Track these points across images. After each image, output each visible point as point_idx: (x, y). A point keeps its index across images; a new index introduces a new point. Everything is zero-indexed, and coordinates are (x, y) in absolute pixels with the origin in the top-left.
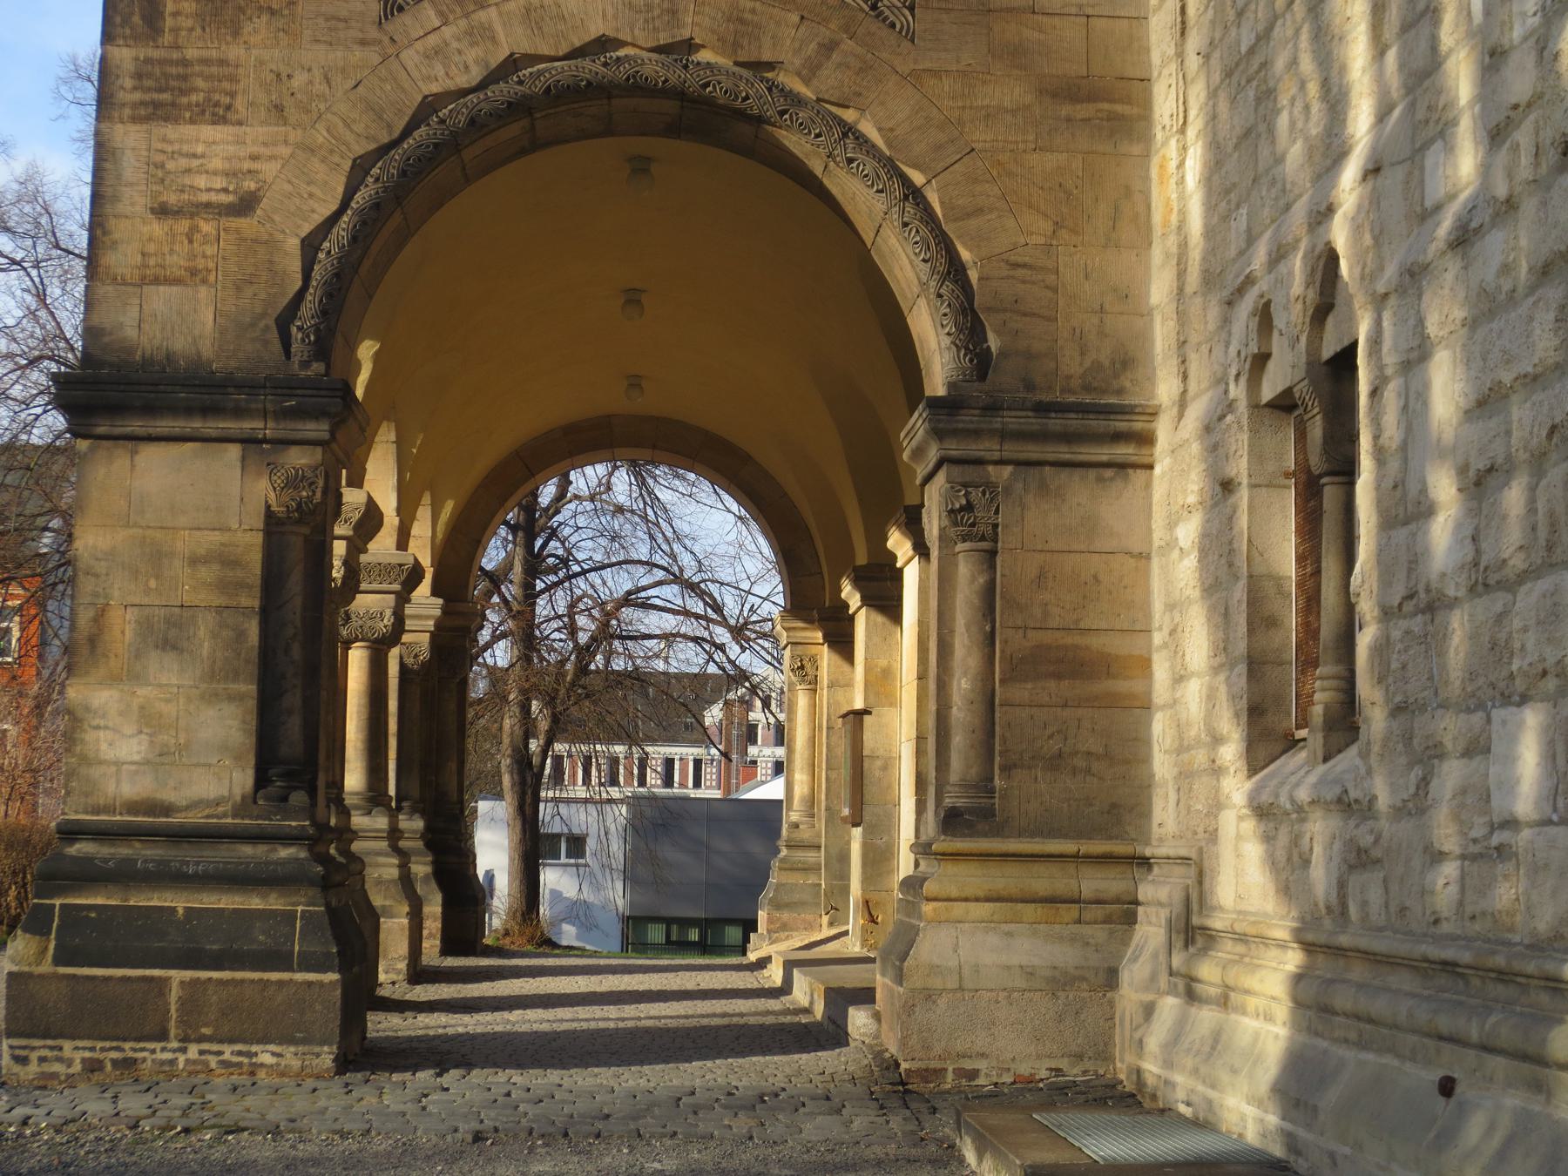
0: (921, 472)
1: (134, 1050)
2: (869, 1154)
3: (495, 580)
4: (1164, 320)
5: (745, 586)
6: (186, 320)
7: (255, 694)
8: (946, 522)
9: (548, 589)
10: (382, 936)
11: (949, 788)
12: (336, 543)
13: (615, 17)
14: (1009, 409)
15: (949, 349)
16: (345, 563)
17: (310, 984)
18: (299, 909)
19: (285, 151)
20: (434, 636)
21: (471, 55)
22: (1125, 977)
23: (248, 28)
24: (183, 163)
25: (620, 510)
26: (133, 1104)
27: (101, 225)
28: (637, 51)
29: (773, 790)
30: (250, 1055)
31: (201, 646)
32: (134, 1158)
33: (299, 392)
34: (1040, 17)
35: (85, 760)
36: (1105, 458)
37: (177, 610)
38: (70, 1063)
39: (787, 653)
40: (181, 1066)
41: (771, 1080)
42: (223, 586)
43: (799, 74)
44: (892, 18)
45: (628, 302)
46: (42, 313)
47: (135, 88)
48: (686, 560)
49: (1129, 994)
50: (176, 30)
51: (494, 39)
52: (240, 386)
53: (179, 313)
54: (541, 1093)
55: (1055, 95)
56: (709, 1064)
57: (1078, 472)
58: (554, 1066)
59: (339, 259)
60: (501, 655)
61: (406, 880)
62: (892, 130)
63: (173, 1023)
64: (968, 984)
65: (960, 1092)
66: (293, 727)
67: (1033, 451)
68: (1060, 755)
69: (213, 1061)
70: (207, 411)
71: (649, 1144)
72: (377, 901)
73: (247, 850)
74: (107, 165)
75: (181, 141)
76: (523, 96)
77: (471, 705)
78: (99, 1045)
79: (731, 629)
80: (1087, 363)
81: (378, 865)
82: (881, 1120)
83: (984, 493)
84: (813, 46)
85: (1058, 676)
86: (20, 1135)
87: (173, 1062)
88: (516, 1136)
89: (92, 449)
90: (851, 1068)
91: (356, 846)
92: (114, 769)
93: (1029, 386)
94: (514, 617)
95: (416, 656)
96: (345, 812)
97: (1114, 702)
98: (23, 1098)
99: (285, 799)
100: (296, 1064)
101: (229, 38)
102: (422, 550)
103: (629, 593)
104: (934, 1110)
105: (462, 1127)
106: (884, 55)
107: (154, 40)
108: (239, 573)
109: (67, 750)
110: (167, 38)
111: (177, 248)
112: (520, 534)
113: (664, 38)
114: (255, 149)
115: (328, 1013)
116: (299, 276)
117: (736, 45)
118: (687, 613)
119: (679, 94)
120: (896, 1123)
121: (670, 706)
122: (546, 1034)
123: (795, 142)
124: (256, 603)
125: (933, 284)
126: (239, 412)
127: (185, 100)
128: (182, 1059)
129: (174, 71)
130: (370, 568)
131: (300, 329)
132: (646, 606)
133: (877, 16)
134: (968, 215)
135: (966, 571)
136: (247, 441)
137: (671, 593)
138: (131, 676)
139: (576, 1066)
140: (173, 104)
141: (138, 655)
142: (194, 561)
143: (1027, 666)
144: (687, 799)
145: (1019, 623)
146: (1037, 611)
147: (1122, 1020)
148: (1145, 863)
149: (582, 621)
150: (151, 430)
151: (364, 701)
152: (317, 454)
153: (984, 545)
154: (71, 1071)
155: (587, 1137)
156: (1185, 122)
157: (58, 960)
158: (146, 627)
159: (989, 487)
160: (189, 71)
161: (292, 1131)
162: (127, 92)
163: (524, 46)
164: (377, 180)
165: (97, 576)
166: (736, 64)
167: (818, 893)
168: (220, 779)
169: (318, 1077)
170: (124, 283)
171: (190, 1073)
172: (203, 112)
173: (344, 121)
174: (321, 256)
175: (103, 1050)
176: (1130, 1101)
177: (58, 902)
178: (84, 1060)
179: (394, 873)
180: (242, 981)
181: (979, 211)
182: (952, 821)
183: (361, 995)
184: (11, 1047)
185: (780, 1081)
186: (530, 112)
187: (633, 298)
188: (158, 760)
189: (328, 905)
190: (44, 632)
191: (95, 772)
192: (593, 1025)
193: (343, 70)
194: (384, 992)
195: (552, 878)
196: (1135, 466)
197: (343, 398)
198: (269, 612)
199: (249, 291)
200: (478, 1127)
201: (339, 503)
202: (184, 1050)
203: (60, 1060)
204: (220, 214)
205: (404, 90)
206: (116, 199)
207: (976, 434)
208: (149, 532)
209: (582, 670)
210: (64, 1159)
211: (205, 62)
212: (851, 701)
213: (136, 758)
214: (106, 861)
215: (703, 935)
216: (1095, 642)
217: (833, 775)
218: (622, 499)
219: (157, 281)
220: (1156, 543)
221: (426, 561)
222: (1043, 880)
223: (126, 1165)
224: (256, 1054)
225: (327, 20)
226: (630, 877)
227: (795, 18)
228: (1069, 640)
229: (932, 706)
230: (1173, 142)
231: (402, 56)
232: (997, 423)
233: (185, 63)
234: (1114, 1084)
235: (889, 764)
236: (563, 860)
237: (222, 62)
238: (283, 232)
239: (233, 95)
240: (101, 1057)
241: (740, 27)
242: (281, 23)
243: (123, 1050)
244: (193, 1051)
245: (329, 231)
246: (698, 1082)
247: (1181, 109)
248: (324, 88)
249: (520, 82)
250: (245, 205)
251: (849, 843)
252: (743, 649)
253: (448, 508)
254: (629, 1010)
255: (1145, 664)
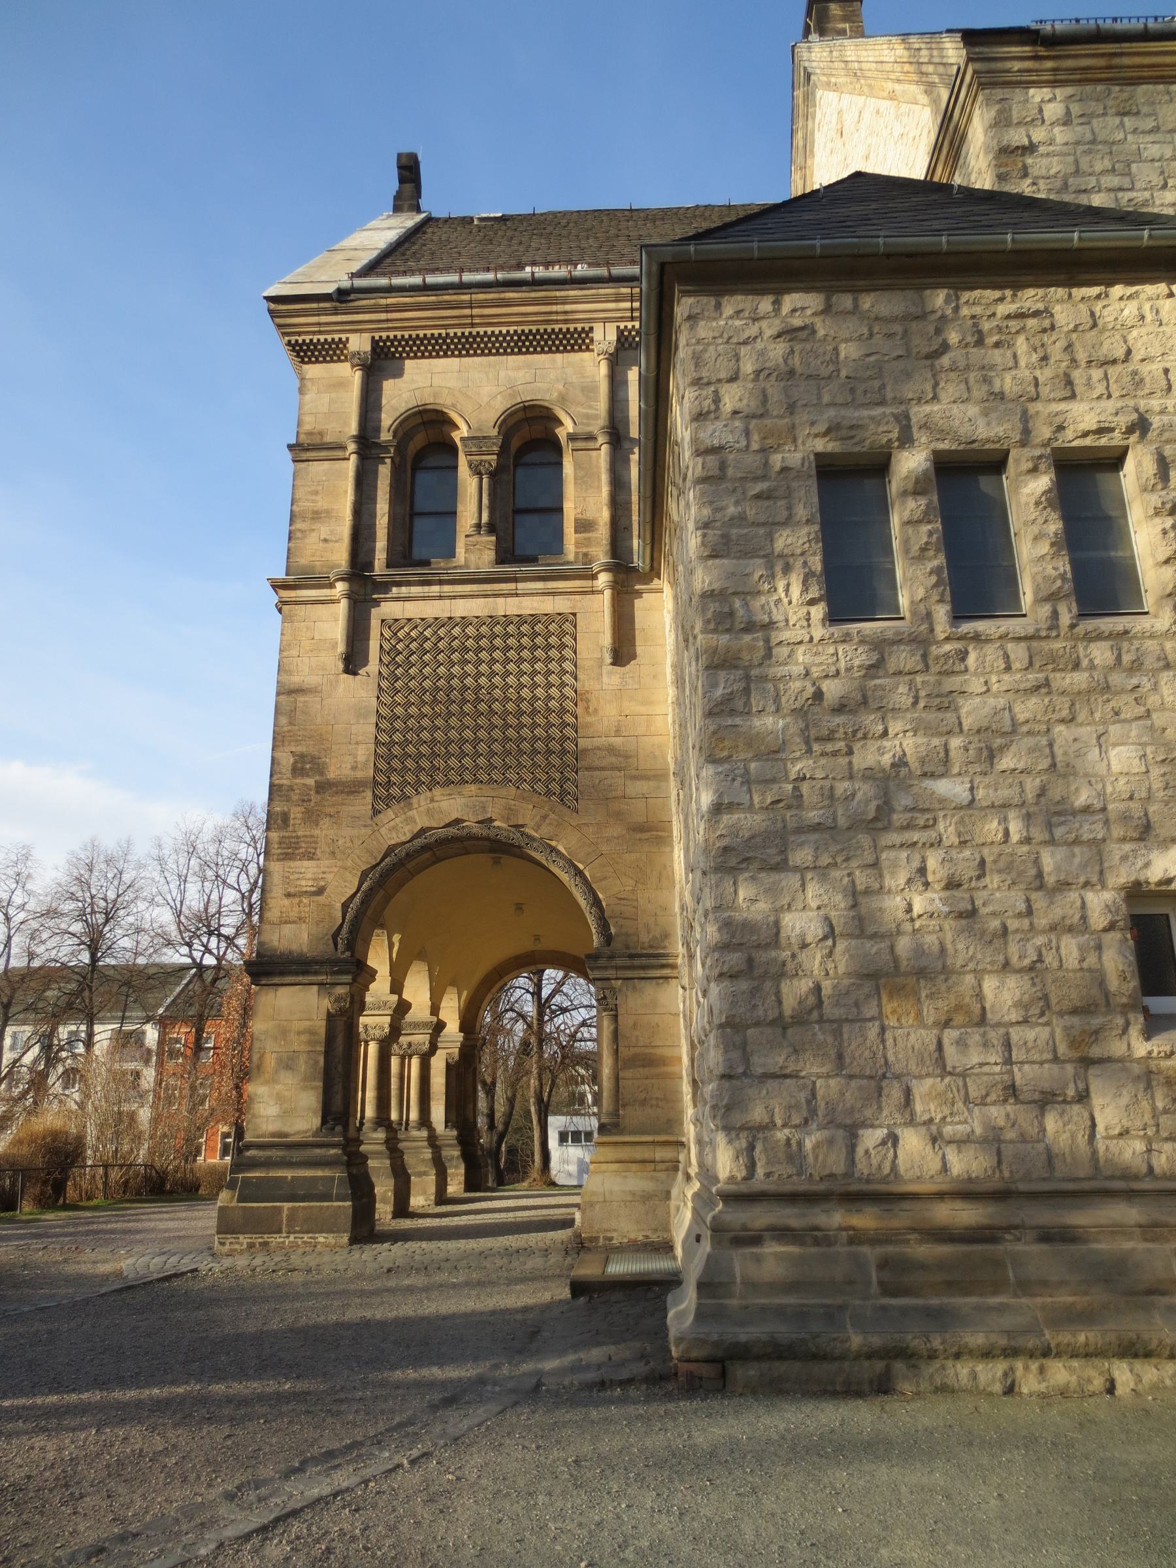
6: (295, 936)
21: (407, 829)
35: (254, 1116)
42: (310, 1043)
52: (316, 963)
66: (338, 1100)
67: (629, 974)
70: (305, 973)
73: (318, 1151)
93: (628, 947)
115: (346, 1220)
119: (487, 839)
126: (316, 973)
136: (320, 984)
138: (274, 1081)
141: (276, 1072)
142: (299, 1033)
158: (279, 1061)
159: (612, 989)
162: (275, 850)
163: (427, 824)
187: (519, 907)
191: (258, 1121)
198: (327, 1054)
207: (605, 968)
216: (658, 1051)
228: (647, 1051)
241: (510, 812)
250: (320, 891)
253: (465, 993)
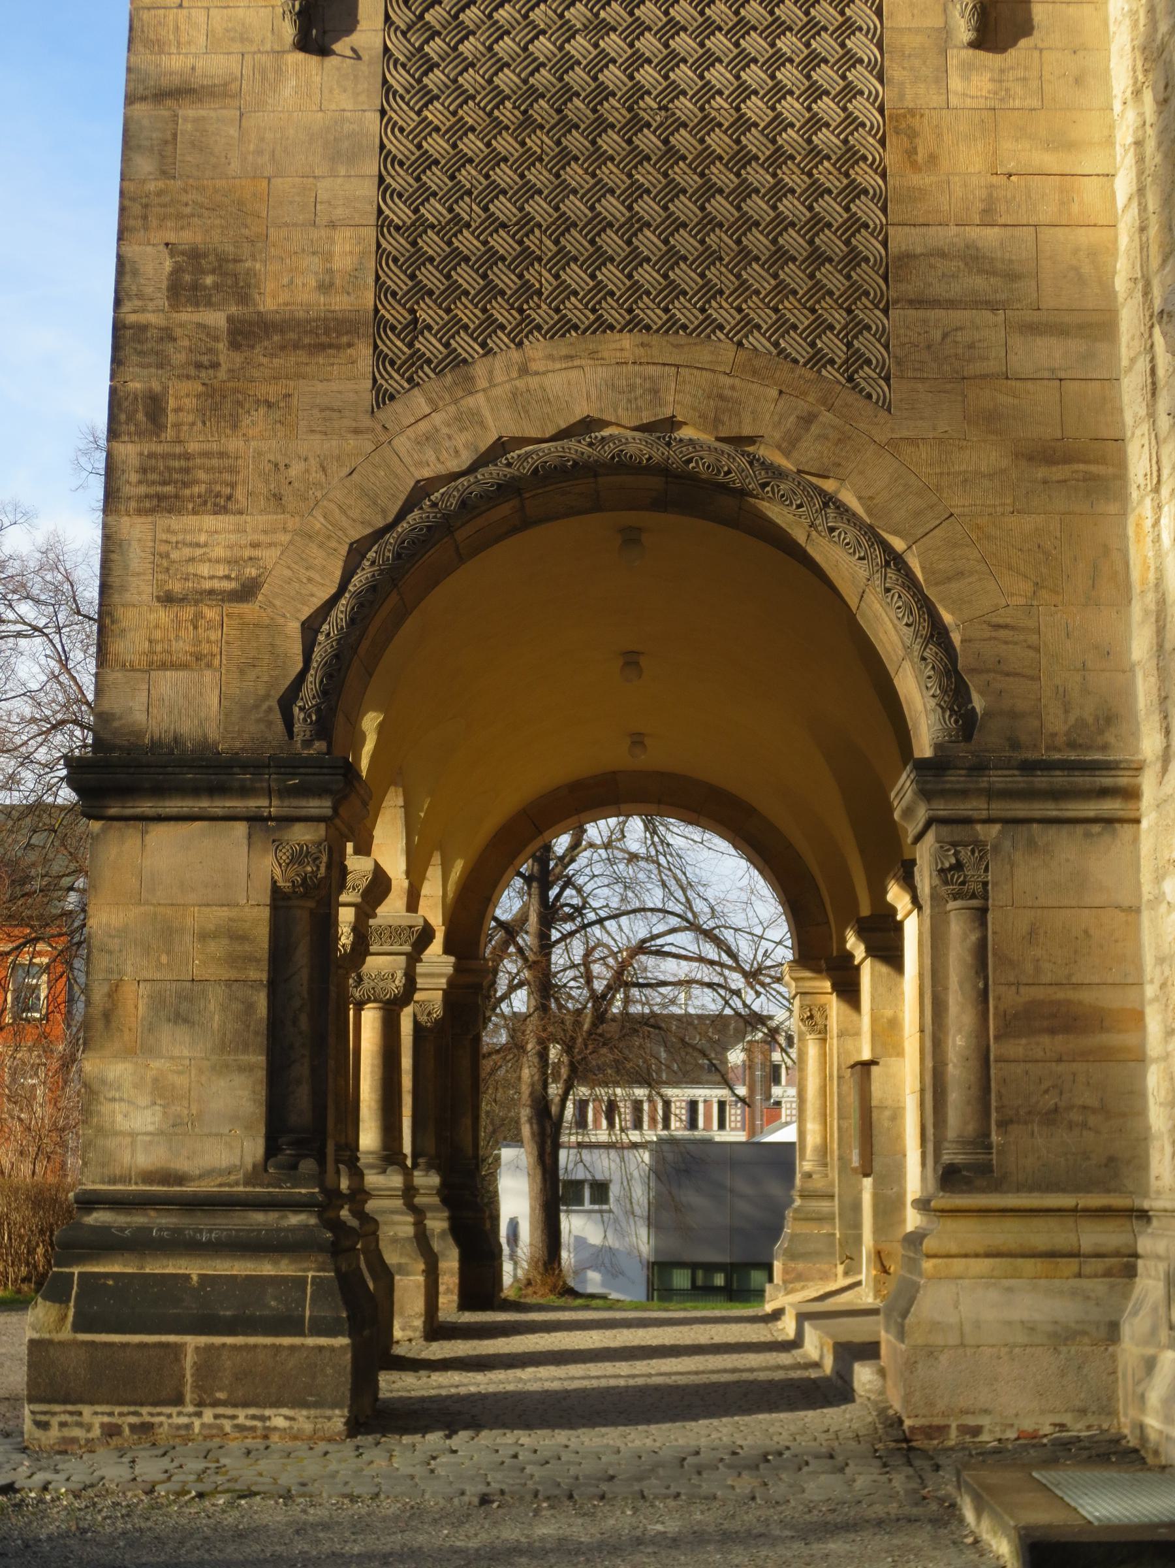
0: (912, 830)
1: (152, 1415)
2: (870, 1513)
3: (510, 930)
4: (1145, 676)
5: (758, 931)
6: (191, 704)
7: (264, 1065)
8: (937, 881)
9: (564, 938)
10: (397, 1294)
11: (947, 1145)
12: (342, 910)
13: (599, 398)
14: (996, 768)
15: (934, 710)
16: (355, 929)
17: (321, 1348)
18: (310, 1274)
19: (285, 538)
20: (446, 993)
21: (461, 440)
22: (1126, 1330)
23: (246, 421)
24: (187, 552)
25: (633, 857)
26: (150, 1468)
27: (110, 614)
28: (622, 430)
29: (786, 1134)
30: (263, 1418)
31: (212, 1019)
32: (149, 1524)
33: (302, 770)
34: (1013, 383)
35: (100, 1130)
36: (1091, 814)
37: (188, 984)
38: (89, 1428)
39: (797, 1002)
40: (197, 1430)
41: (775, 1438)
42: (233, 960)
43: (779, 447)
44: (868, 389)
45: (627, 664)
46: (64, 678)
47: (140, 482)
48: (699, 906)
49: (1130, 1349)
50: (178, 425)
51: (482, 424)
52: (245, 766)
53: (186, 697)
54: (547, 1454)
55: (1031, 459)
56: (715, 1422)
57: (1066, 829)
58: (561, 1426)
59: (339, 641)
60: (520, 1001)
61: (422, 1238)
62: (871, 498)
63: (188, 1388)
64: (970, 1340)
65: (963, 1449)
66: (302, 1097)
67: (1020, 809)
68: (1056, 1109)
69: (227, 1425)
71: (652, 1506)
72: (392, 1258)
73: (259, 1217)
74: (114, 556)
75: (185, 531)
76: (513, 478)
77: (484, 1057)
78: (117, 1410)
79: (745, 974)
80: (1072, 720)
81: (394, 1223)
82: (884, 1478)
83: (973, 852)
84: (792, 419)
85: (1052, 1031)
86: (41, 1501)
87: (188, 1427)
88: (521, 1499)
89: (104, 830)
90: (855, 1426)
91: (371, 1206)
92: (129, 1140)
93: (1015, 745)
94: (530, 968)
95: (429, 1014)
96: (357, 1174)
97: (1107, 1055)
98: (44, 1463)
99: (294, 1167)
100: (308, 1427)
101: (228, 431)
102: (432, 912)
103: (644, 941)
104: (937, 1468)
105: (470, 1489)
106: (862, 426)
107: (158, 436)
108: (247, 948)
109: (85, 1122)
110: (170, 433)
111: (182, 633)
112: (535, 884)
113: (646, 418)
114: (256, 537)
116: (300, 658)
117: (717, 421)
118: (701, 959)
119: (662, 470)
120: (899, 1481)
121: (692, 1049)
122: (556, 1392)
123: (777, 513)
124: (264, 977)
125: (916, 647)
126: (245, 792)
127: (187, 492)
128: (197, 1423)
129: (176, 464)
130: (380, 931)
131: (301, 709)
132: (660, 953)
133: (854, 388)
134: (949, 579)
135: (958, 928)
136: (253, 819)
137: (685, 941)
138: (144, 1049)
139: (584, 1426)
140: (177, 496)
142: (204, 936)
143: (1017, 1023)
144: (709, 1142)
145: (1012, 979)
146: (1029, 967)
147: (1125, 1375)
148: (1144, 1215)
149: (596, 968)
150: (160, 811)
151: (378, 1061)
152: (321, 830)
153: (975, 903)
154: (90, 1436)
155: (591, 1498)
156: (1159, 481)
157: (77, 1328)
158: (158, 1002)
159: (978, 845)
160: (191, 464)
161: (303, 1495)
162: (132, 484)
163: (512, 429)
164: (373, 563)
165: (110, 952)
166: (718, 439)
167: (832, 1244)
168: (231, 1148)
169: (330, 1440)
170: (133, 670)
171: (205, 1438)
172: (205, 503)
173: (340, 507)
174: (321, 638)
175: (121, 1414)
176: (1133, 1456)
177: (76, 1270)
178: (102, 1425)
179: (410, 1231)
180: (255, 1346)
181: (960, 574)
182: (949, 1177)
183: (374, 1351)
184: (32, 1412)
185: (784, 1440)
186: (518, 492)
187: (631, 661)
188: (171, 1130)
189: (337, 1271)
190: (71, 988)
191: (111, 1143)
192: (603, 1383)
193: (338, 458)
194: (398, 1350)
195: (576, 1225)
196: (1122, 821)
197: (345, 775)
199: (251, 675)
200: (482, 1488)
201: (344, 872)
202: (199, 1415)
203: (80, 1425)
204: (223, 600)
205: (396, 476)
206: (124, 588)
207: (964, 794)
208: (160, 909)
209: (600, 1017)
210: (81, 1524)
211: (206, 454)
212: (859, 1051)
213: (151, 1128)
214: (122, 1229)
215: (728, 1280)
216: (1086, 997)
217: (845, 1124)
218: (634, 846)
219: (163, 666)
220: (1146, 897)
221: (436, 920)
222: (1041, 1235)
223: (141, 1530)
224: (269, 1418)
225: (322, 410)
226: (653, 1223)
227: (774, 393)
228: (1061, 995)
229: (929, 1064)
230: (1148, 502)
231: (394, 442)
232: (983, 782)
233: (187, 456)
234: (1118, 1440)
235: (897, 1115)
236: (587, 1206)
237: (222, 455)
238: (284, 616)
239: (233, 485)
240: (119, 1421)
242: (277, 415)
243: (140, 1415)
244: (208, 1415)
245: (328, 614)
246: (703, 1442)
247: (1155, 468)
248: (320, 476)
249: (509, 465)
250: (247, 591)
251: (860, 1192)
252: (758, 994)
253: (458, 867)
254: (641, 1367)
255: (1138, 1017)
